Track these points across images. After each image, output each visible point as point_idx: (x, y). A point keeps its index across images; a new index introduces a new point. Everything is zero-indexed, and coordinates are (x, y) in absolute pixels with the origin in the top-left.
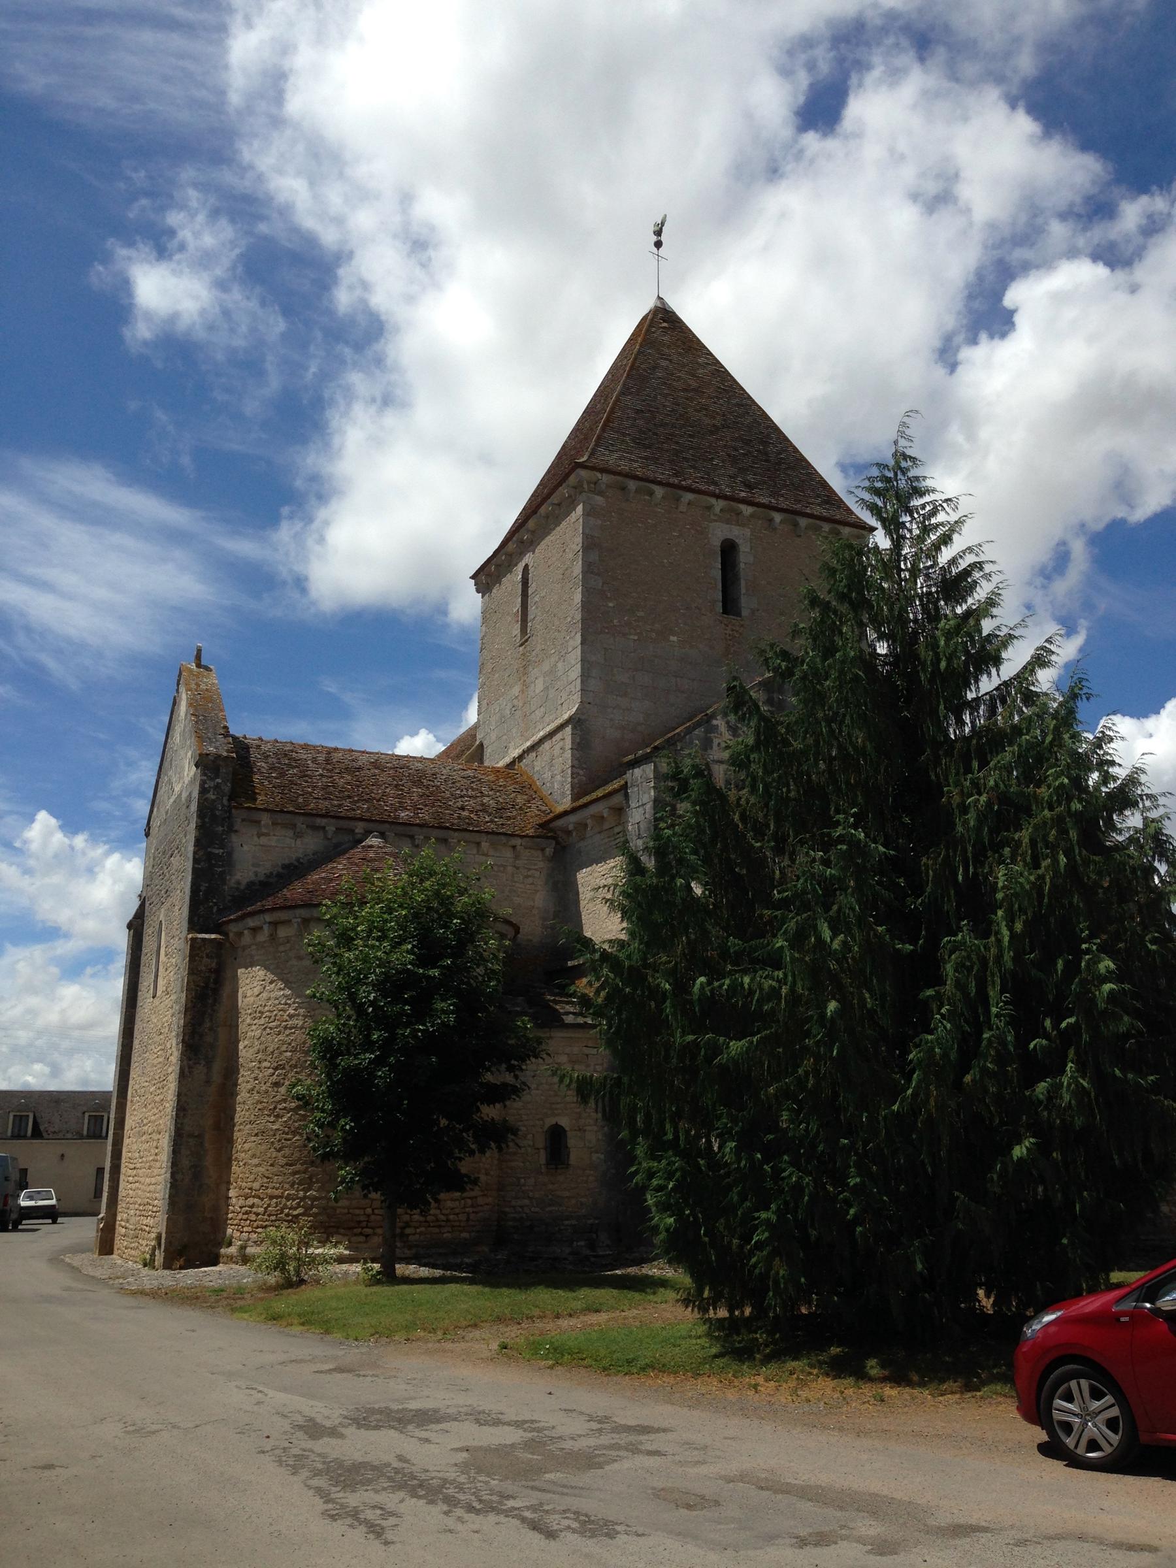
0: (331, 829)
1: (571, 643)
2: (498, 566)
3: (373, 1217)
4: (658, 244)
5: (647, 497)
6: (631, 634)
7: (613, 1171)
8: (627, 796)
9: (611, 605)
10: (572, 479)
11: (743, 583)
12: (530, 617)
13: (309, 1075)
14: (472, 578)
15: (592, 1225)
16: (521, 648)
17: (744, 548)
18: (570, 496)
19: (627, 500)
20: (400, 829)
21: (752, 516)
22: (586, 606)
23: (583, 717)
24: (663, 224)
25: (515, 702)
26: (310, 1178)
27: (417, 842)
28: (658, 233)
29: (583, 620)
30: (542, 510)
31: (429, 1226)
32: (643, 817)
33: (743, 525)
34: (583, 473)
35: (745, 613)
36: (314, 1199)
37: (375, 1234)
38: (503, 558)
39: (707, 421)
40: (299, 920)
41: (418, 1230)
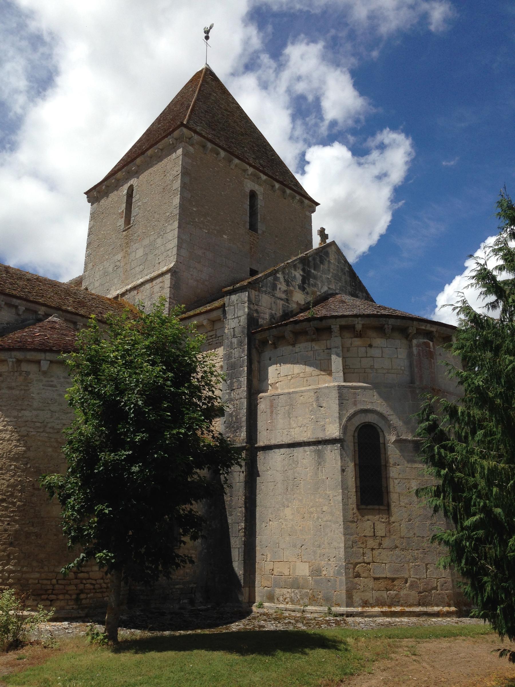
0: (22, 309)
1: (169, 228)
2: (107, 186)
3: (57, 586)
4: (207, 38)
5: (215, 155)
6: (204, 229)
7: (206, 551)
8: (224, 312)
9: (195, 209)
10: (176, 134)
11: (259, 217)
12: (133, 213)
13: (12, 476)
14: (86, 193)
15: (192, 588)
16: (124, 233)
17: (260, 197)
18: (173, 144)
19: (205, 153)
20: (69, 316)
21: (265, 181)
22: (182, 206)
23: (177, 270)
24: (211, 28)
25: (118, 264)
26: (8, 555)
27: (78, 327)
28: (207, 32)
29: (180, 214)
30: (149, 152)
31: (96, 592)
32: (238, 325)
33: (260, 185)
34: (185, 130)
35: (260, 232)
36: (10, 572)
37: (58, 599)
38: (113, 181)
39: (238, 129)
40: (14, 360)
41: (89, 596)
